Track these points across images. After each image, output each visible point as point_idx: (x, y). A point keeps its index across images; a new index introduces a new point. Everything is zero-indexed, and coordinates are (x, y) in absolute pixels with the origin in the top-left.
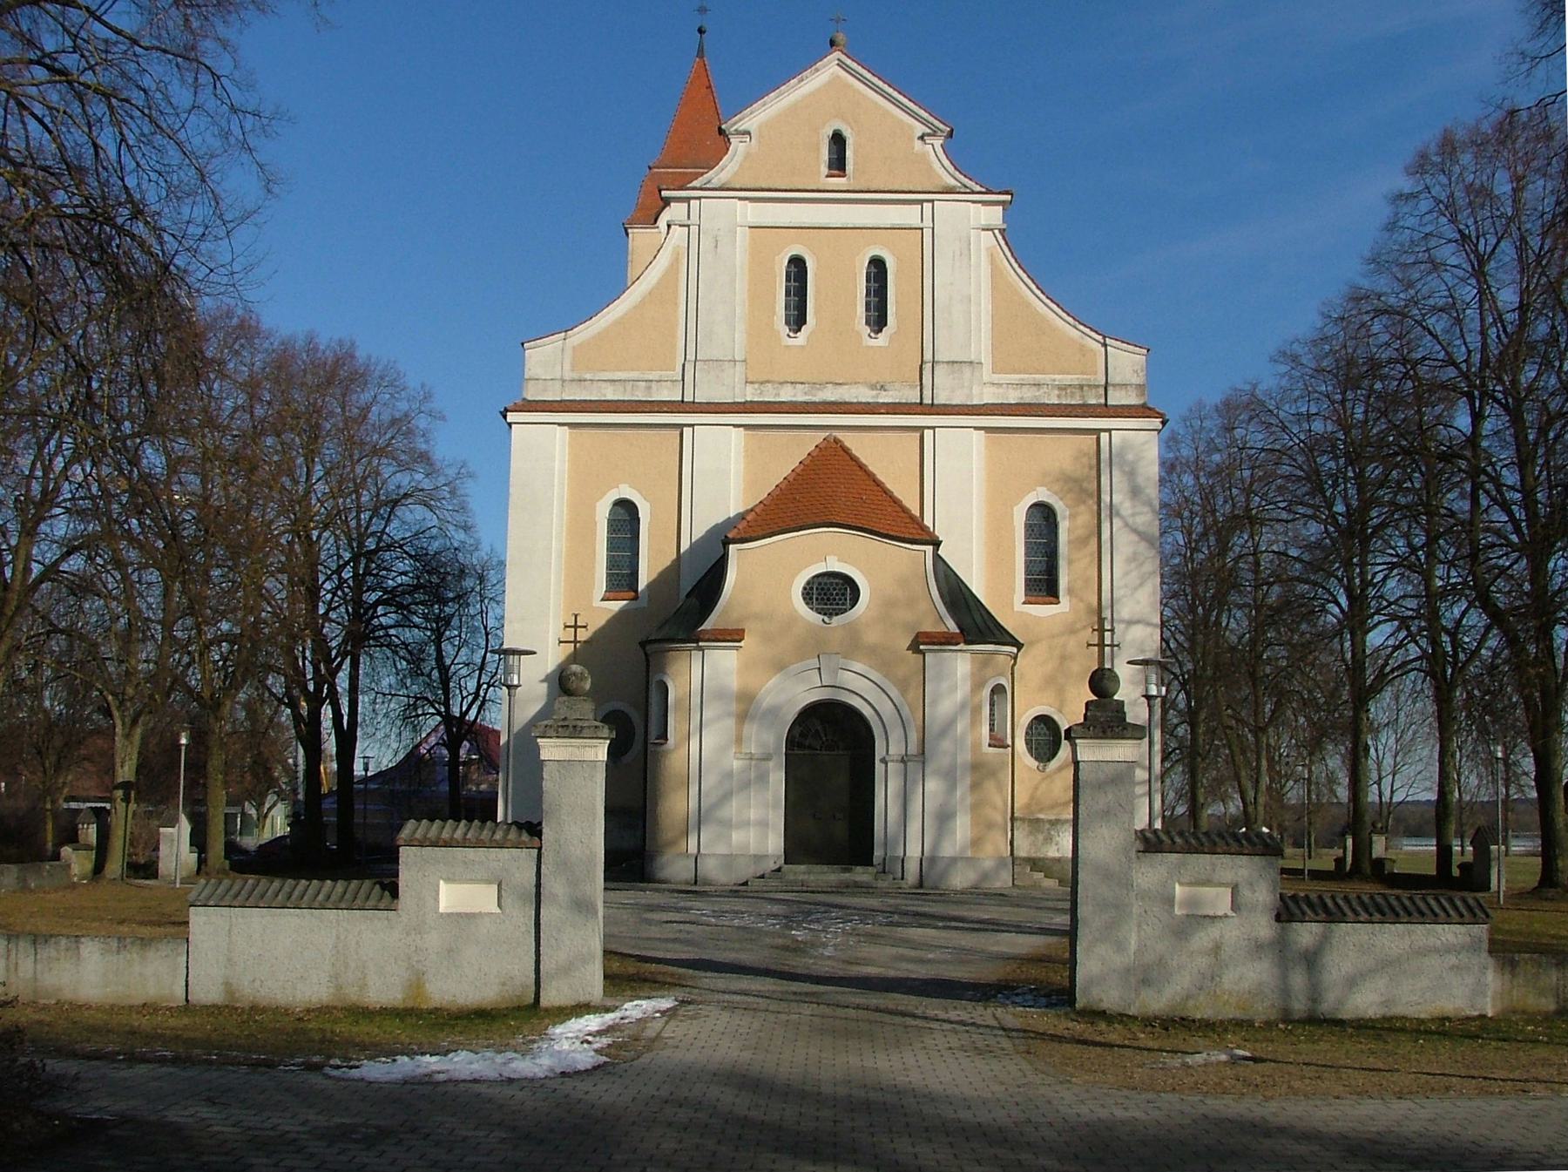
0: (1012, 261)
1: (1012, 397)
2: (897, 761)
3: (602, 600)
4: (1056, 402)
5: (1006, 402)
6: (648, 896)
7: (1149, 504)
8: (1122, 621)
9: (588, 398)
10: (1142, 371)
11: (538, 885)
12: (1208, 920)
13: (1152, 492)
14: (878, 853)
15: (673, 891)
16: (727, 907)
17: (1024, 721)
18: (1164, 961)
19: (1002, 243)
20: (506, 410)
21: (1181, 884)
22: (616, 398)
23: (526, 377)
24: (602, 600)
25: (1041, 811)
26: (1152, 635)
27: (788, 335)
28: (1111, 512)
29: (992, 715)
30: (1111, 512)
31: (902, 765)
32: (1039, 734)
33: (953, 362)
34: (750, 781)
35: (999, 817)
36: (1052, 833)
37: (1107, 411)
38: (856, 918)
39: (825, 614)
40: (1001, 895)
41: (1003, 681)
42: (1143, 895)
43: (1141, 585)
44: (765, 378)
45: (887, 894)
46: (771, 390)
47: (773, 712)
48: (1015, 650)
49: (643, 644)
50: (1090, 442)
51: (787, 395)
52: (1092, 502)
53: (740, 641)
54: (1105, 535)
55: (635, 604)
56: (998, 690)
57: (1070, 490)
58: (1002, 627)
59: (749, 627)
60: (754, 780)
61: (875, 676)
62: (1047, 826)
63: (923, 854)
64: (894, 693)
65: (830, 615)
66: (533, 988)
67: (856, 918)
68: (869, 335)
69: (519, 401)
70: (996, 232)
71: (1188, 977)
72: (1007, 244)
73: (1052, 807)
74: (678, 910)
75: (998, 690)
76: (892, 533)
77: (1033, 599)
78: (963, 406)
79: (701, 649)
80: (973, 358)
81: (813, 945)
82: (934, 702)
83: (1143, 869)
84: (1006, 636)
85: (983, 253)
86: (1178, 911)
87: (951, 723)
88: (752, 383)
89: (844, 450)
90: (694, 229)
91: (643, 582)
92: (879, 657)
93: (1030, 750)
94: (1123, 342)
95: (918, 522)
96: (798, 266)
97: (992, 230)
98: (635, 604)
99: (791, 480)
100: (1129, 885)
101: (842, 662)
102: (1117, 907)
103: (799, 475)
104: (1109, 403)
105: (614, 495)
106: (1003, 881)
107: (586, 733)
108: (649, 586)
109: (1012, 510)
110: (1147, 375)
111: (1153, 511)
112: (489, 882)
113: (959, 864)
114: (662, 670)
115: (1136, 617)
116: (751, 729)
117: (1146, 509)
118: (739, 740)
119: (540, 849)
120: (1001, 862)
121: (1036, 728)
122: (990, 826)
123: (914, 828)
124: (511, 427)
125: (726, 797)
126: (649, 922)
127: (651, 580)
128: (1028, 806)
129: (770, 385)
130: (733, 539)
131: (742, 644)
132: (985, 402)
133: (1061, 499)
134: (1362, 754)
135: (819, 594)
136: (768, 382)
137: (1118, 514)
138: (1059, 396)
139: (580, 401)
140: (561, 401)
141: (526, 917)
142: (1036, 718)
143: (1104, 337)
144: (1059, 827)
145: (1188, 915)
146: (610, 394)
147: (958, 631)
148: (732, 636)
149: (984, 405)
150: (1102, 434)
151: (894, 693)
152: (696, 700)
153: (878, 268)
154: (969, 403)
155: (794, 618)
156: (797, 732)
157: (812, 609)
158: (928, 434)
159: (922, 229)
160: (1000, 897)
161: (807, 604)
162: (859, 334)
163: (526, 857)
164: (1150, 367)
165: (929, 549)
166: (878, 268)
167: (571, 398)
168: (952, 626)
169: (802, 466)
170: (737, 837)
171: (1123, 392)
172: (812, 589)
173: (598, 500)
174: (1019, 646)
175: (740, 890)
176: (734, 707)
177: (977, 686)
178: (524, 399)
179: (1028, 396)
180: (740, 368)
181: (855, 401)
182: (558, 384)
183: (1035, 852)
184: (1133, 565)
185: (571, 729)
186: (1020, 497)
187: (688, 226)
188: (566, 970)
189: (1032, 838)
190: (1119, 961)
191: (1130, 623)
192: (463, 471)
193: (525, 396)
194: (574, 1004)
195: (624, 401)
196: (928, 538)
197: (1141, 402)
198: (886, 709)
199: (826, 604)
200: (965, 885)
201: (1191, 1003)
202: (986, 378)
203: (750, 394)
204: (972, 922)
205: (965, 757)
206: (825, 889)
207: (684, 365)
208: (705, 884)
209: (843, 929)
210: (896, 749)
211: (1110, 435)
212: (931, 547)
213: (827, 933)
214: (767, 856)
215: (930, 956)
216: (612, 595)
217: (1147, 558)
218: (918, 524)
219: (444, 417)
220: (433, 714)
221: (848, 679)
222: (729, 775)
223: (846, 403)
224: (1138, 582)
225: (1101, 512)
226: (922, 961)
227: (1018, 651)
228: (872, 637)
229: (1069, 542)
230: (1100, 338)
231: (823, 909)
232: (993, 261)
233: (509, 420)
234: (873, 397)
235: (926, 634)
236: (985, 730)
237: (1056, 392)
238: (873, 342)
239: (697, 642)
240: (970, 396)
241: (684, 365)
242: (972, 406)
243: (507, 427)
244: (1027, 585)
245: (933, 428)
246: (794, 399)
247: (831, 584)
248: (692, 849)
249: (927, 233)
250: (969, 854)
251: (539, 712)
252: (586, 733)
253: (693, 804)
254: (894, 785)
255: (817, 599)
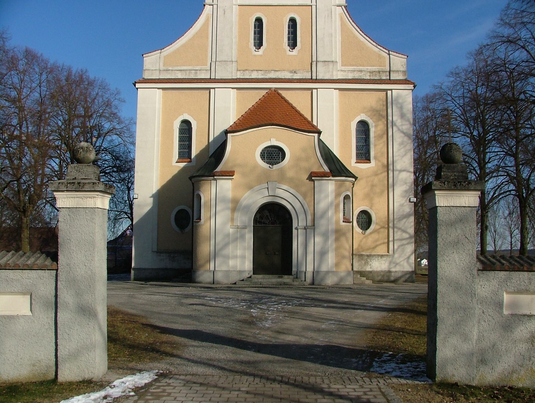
0: (350, 19)
1: (350, 76)
2: (302, 229)
3: (355, 163)
4: (369, 78)
5: (347, 78)
6: (190, 290)
7: (408, 120)
8: (397, 170)
9: (170, 78)
10: (405, 65)
11: (56, 296)
12: (526, 318)
13: (410, 116)
14: (294, 269)
15: (201, 287)
16: (223, 296)
17: (356, 212)
18: (496, 347)
19: (345, 12)
20: (136, 83)
21: (508, 293)
22: (182, 78)
23: (144, 69)
24: (176, 162)
25: (363, 251)
26: (410, 176)
27: (255, 50)
28: (392, 124)
29: (344, 208)
30: (392, 124)
31: (305, 230)
32: (362, 218)
33: (325, 61)
34: (237, 237)
35: (347, 254)
36: (368, 260)
37: (390, 81)
38: (284, 301)
39: (270, 164)
40: (350, 288)
41: (349, 193)
42: (482, 301)
43: (405, 155)
44: (245, 68)
45: (299, 288)
46: (248, 73)
47: (247, 208)
48: (354, 180)
49: (190, 178)
50: (383, 95)
51: (255, 75)
52: (384, 120)
53: (232, 176)
54: (390, 134)
55: (190, 164)
56: (347, 197)
57: (374, 115)
58: (348, 170)
59: (237, 171)
60: (239, 237)
61: (292, 191)
62: (366, 257)
63: (314, 270)
64: (301, 198)
65: (273, 165)
66: (54, 368)
67: (284, 301)
68: (289, 50)
69: (141, 79)
70: (343, 7)
71: (513, 358)
72: (347, 12)
73: (368, 249)
74: (200, 297)
75: (347, 197)
76: (300, 128)
77: (359, 161)
78: (329, 80)
79: (216, 180)
80: (333, 60)
81: (261, 320)
82: (318, 203)
83: (481, 283)
84: (350, 174)
85: (337, 16)
86: (506, 312)
87: (325, 212)
88: (240, 70)
89: (278, 94)
90: (215, 6)
91: (194, 153)
92: (295, 184)
93: (358, 225)
94: (397, 53)
95: (310, 123)
96: (259, 22)
97: (341, 6)
98: (190, 164)
99: (255, 106)
100: (473, 294)
101: (279, 185)
102: (465, 310)
103: (259, 104)
104: (391, 79)
105: (181, 118)
106: (349, 281)
107: (87, 188)
108: (197, 156)
109: (350, 123)
110: (407, 67)
111: (410, 124)
112: (23, 293)
113: (330, 274)
114: (199, 189)
115: (403, 169)
116: (237, 215)
117: (407, 123)
118: (232, 220)
119: (57, 270)
120: (348, 273)
121: (361, 216)
122: (344, 257)
123: (310, 257)
124: (137, 90)
125: (226, 245)
126: (182, 304)
127: (197, 153)
128: (357, 249)
129: (247, 71)
130: (230, 131)
131: (233, 177)
132: (339, 78)
133: (371, 119)
134: (484, 229)
135: (268, 155)
136: (246, 70)
137: (395, 125)
138: (370, 76)
139: (167, 79)
140: (159, 79)
141: (48, 318)
142: (360, 212)
143: (389, 51)
144: (371, 258)
145: (512, 315)
146: (180, 76)
147: (329, 171)
148: (229, 174)
149: (338, 79)
150: (388, 91)
151: (301, 198)
152: (213, 202)
153: (293, 23)
154: (332, 79)
155: (256, 166)
156: (258, 216)
157: (264, 162)
158: (315, 91)
159: (312, 6)
160: (349, 289)
161: (262, 160)
162: (285, 51)
163: (47, 276)
164: (408, 64)
165: (316, 135)
166: (293, 23)
167: (163, 78)
168: (326, 169)
169: (260, 101)
170: (231, 263)
171: (397, 74)
172: (264, 153)
173: (174, 121)
174: (356, 178)
175: (230, 288)
176: (230, 205)
177: (338, 195)
178: (143, 78)
179: (357, 75)
180: (234, 64)
181: (284, 78)
182: (158, 72)
183: (361, 268)
184: (402, 146)
185: (76, 185)
186: (356, 116)
187: (213, 5)
188: (74, 356)
189: (360, 263)
190: (465, 347)
191: (401, 171)
192: (132, 121)
193: (144, 77)
194: (81, 380)
195: (185, 79)
196: (315, 130)
197: (405, 78)
198: (297, 206)
199: (270, 160)
200: (333, 283)
201: (515, 376)
202: (339, 68)
203: (239, 75)
204: (340, 303)
205: (332, 227)
206: (270, 286)
207: (211, 63)
208: (218, 284)
209: (277, 308)
210: (302, 224)
211: (392, 92)
212: (317, 134)
213: (269, 311)
214: (245, 271)
215: (323, 326)
216: (181, 160)
217: (408, 144)
218: (311, 124)
219: (125, 101)
220: (126, 218)
221: (280, 192)
222: (228, 235)
223: (280, 79)
224: (404, 153)
225: (388, 124)
226: (319, 330)
227: (355, 180)
228: (290, 174)
229: (375, 137)
230: (387, 51)
231: (268, 296)
232: (341, 19)
233: (136, 87)
234: (291, 76)
235: (315, 173)
236: (341, 215)
237: (369, 74)
238: (291, 53)
239: (214, 176)
240: (332, 75)
241: (211, 63)
242: (333, 80)
243: (136, 89)
244: (357, 155)
245: (317, 89)
246: (257, 77)
247: (273, 151)
248: (212, 268)
249: (314, 7)
250: (334, 270)
251: (150, 210)
252: (87, 188)
253: (212, 248)
254: (301, 239)
255: (267, 158)
